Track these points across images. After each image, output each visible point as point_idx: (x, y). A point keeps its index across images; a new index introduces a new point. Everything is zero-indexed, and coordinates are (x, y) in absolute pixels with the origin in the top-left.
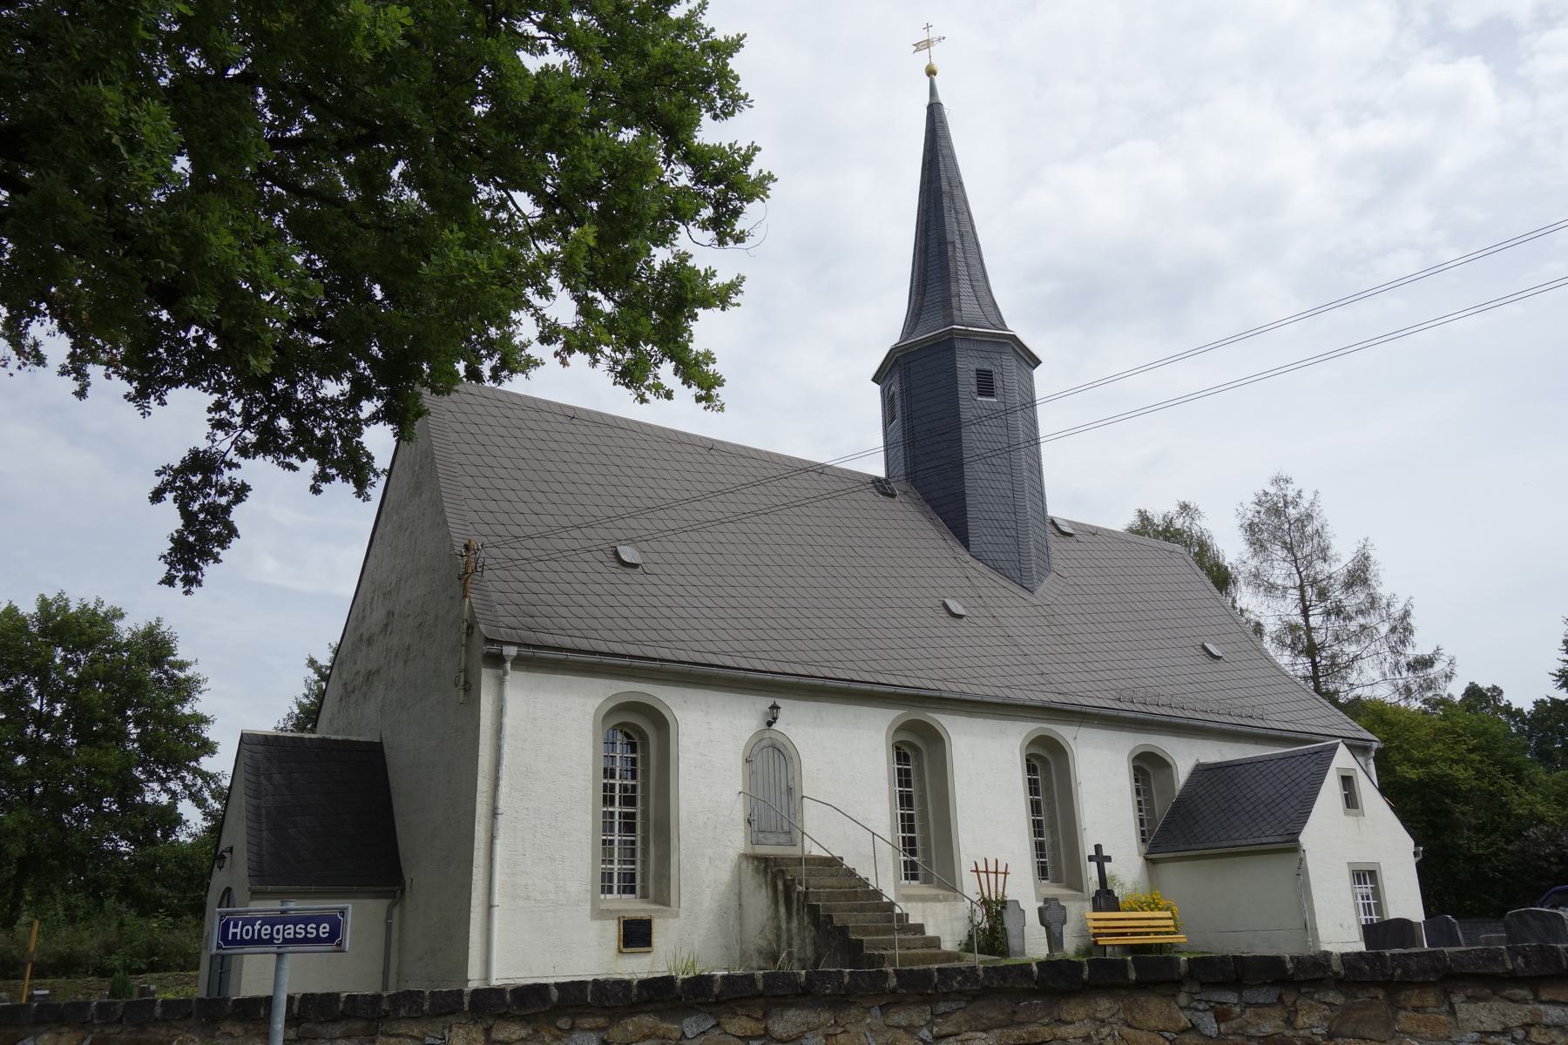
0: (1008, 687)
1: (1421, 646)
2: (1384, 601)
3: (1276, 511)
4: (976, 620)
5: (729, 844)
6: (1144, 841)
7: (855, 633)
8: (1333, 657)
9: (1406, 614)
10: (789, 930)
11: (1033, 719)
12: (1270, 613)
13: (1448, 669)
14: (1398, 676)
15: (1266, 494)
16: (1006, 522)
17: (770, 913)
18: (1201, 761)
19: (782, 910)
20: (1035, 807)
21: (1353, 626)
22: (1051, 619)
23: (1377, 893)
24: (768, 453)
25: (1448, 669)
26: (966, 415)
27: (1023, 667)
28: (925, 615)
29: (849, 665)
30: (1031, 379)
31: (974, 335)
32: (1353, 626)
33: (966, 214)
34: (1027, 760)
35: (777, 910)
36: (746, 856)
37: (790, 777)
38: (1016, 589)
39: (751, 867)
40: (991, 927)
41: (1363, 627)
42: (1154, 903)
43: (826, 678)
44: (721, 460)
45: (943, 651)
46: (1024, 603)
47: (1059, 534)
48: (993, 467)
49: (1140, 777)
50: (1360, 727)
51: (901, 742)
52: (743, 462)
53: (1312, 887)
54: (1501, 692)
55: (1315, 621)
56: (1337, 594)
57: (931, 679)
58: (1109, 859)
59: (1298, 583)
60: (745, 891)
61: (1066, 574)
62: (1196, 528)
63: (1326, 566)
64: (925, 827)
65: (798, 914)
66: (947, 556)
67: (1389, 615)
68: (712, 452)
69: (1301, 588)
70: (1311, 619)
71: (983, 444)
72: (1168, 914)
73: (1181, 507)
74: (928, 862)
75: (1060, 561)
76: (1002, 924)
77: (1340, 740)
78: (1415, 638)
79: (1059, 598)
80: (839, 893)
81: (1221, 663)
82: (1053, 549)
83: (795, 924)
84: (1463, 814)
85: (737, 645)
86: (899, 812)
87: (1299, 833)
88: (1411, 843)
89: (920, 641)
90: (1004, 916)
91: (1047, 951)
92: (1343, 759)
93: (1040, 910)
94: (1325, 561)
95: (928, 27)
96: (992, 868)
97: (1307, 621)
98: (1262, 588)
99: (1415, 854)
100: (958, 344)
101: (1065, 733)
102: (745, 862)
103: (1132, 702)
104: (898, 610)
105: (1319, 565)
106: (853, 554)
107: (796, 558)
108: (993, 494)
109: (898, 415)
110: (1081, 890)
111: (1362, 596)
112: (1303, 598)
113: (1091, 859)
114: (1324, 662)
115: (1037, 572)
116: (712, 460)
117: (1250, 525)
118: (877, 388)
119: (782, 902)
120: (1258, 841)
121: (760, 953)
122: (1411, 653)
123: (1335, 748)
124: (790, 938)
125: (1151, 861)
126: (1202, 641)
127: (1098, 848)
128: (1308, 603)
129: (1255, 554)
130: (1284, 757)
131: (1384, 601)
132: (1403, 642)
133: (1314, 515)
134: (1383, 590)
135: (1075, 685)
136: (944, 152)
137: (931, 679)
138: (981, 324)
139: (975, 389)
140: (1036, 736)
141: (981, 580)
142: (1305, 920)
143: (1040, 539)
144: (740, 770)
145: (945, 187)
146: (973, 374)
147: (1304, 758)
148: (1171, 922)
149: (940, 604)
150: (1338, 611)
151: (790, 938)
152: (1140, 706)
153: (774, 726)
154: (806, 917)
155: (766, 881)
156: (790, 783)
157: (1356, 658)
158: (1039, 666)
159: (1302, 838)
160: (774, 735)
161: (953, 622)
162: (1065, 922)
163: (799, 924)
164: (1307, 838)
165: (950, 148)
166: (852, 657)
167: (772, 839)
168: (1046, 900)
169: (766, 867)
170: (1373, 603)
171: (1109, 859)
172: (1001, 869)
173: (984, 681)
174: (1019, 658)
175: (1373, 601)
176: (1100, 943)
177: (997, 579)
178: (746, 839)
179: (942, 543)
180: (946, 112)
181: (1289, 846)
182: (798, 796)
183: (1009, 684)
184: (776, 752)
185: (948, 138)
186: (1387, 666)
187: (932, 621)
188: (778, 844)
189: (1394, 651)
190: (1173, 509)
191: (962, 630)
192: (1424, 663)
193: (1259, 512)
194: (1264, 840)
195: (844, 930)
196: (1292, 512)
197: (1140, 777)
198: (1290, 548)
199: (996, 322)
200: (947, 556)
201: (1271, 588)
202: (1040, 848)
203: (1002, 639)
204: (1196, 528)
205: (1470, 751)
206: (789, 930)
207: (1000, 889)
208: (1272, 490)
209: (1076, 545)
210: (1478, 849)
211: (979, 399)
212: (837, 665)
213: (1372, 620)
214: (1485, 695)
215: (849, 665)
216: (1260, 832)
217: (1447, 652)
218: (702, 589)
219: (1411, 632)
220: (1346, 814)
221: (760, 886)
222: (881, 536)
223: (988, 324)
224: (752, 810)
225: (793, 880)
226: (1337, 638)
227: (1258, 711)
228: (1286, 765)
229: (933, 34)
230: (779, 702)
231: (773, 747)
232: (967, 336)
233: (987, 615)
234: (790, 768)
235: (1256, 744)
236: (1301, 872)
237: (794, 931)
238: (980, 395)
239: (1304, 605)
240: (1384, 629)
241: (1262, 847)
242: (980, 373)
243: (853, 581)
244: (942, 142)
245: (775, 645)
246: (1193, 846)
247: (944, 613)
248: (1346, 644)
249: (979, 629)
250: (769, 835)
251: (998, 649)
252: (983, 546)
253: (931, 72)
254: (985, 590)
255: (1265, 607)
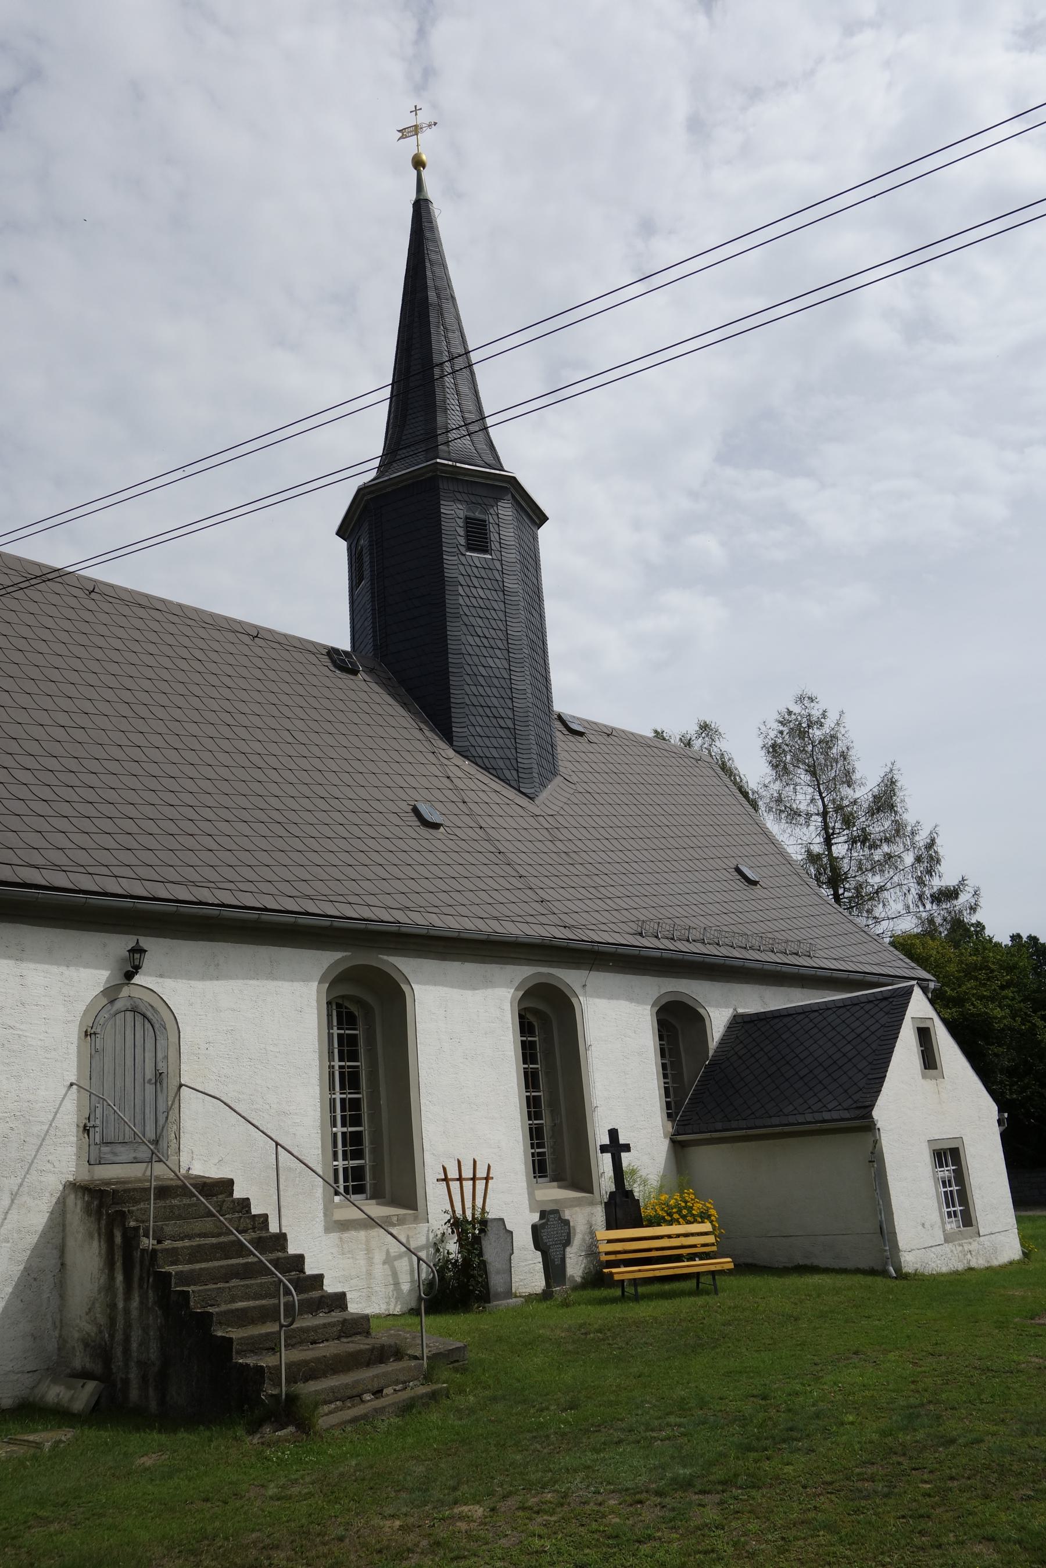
0: (496, 919)
1: (946, 877)
2: (909, 828)
3: (800, 732)
4: (457, 831)
5: (49, 1166)
6: (669, 1116)
7: (279, 843)
8: (859, 888)
9: (931, 845)
10: (127, 1311)
11: (529, 961)
12: (792, 841)
13: (973, 901)
14: (921, 909)
15: (790, 713)
16: (501, 711)
17: (102, 1281)
18: (740, 1011)
19: (119, 1278)
20: (530, 1080)
21: (878, 855)
22: (556, 832)
23: (960, 1177)
24: (180, 605)
25: (973, 901)
26: (450, 572)
27: (517, 892)
28: (387, 823)
29: (265, 887)
30: (535, 538)
31: (465, 475)
32: (878, 855)
33: (458, 333)
34: (521, 1016)
35: (111, 1278)
36: (74, 1187)
37: (160, 1055)
38: (511, 794)
39: (79, 1203)
40: (464, 1259)
41: (889, 857)
42: (686, 1207)
43: (223, 905)
44: (106, 607)
45: (409, 871)
46: (522, 813)
47: (566, 732)
48: (484, 640)
49: (665, 1033)
50: (913, 965)
51: (343, 997)
52: (141, 612)
53: (890, 1178)
54: (984, 928)
55: (840, 849)
56: (862, 821)
57: (387, 908)
58: (627, 1148)
59: (821, 810)
60: (71, 1243)
61: (574, 779)
62: (715, 749)
63: (850, 791)
64: (375, 1116)
65: (141, 1287)
66: (423, 749)
67: (913, 844)
68: (93, 595)
69: (824, 814)
70: (834, 848)
71: (472, 610)
72: (707, 1227)
73: (701, 727)
74: (377, 1169)
75: (568, 764)
76: (481, 1254)
77: (915, 982)
78: (941, 868)
79: (566, 807)
80: (213, 1246)
81: (758, 891)
82: (559, 748)
83: (135, 1303)
84: (996, 1055)
85: (82, 857)
86: (338, 1096)
87: (872, 1106)
88: (994, 1108)
89: (375, 856)
90: (483, 1242)
91: (543, 1283)
92: (919, 1007)
93: (535, 1228)
94: (849, 786)
95: (416, 110)
96: (467, 1173)
97: (830, 850)
98: (783, 816)
99: (1000, 1122)
100: (443, 485)
101: (570, 978)
102: (72, 1196)
103: (657, 937)
104: (348, 815)
105: (845, 791)
106: (290, 739)
107: (203, 740)
108: (484, 674)
109: (367, 573)
110: (590, 1191)
111: (887, 824)
112: (826, 827)
113: (604, 1149)
114: (847, 894)
115: (539, 774)
116: (91, 605)
117: (774, 746)
118: (342, 545)
119: (119, 1265)
120: (818, 1117)
121: (86, 1345)
122: (936, 883)
123: (908, 993)
124: (128, 1326)
125: (678, 1146)
126: (735, 863)
127: (613, 1134)
128: (831, 831)
129: (779, 777)
130: (844, 1005)
131: (909, 828)
132: (929, 872)
133: (840, 736)
134: (909, 818)
135: (584, 915)
136: (433, 256)
137: (387, 908)
138: (471, 461)
139: (462, 541)
140: (531, 985)
141: (467, 781)
142: (881, 1222)
143: (543, 735)
144: (73, 1049)
145: (432, 295)
146: (461, 522)
147: (871, 1005)
148: (711, 1239)
149: (409, 809)
150: (863, 839)
151: (128, 1326)
152: (666, 942)
153: (138, 979)
154: (151, 1293)
155: (99, 1228)
156: (161, 1066)
157: (881, 889)
158: (539, 891)
159: (876, 1113)
160: (136, 993)
161: (425, 832)
162: (568, 1242)
163: (141, 1303)
164: (882, 1112)
165: (440, 253)
166: (270, 876)
167: (125, 1153)
168: (543, 1214)
169: (100, 1206)
170: (898, 831)
171: (627, 1148)
172: (481, 1173)
173: (463, 910)
174: (513, 880)
175: (899, 828)
176: (617, 1277)
177: (487, 780)
178: (79, 1157)
179: (418, 734)
180: (436, 213)
181: (867, 1126)
182: (173, 1084)
183: (497, 914)
184: (139, 1018)
185: (437, 241)
186: (910, 898)
187: (397, 831)
188: (136, 1161)
189: (920, 882)
190: (692, 729)
191: (437, 843)
192: (949, 894)
193: (781, 732)
194: (827, 1116)
195: (205, 1320)
196: (817, 733)
197: (665, 1033)
198: (812, 771)
199: (490, 459)
200: (423, 749)
201: (793, 815)
202: (535, 1135)
203: (491, 856)
204: (715, 749)
205: (1002, 987)
206: (127, 1311)
207: (479, 1202)
208: (796, 709)
209: (587, 745)
210: (1011, 1094)
211: (468, 554)
212: (243, 886)
213: (896, 849)
214: (968, 930)
215: (265, 887)
216: (820, 1105)
217: (972, 883)
218: (274, 854)
219: (938, 861)
220: (924, 1077)
221: (91, 1236)
222: (405, 785)
223: (481, 463)
224: (93, 1110)
225: (137, 1229)
226: (860, 869)
227: (805, 947)
228: (848, 1014)
229: (423, 118)
230: (145, 942)
231: (134, 1010)
232: (455, 475)
233: (473, 824)
234: (161, 1042)
235: (803, 987)
236: (875, 1160)
237: (135, 1313)
238: (469, 549)
239: (827, 832)
240: (909, 859)
241: (825, 1126)
242: (469, 522)
243: (287, 774)
244: (430, 246)
245: (148, 857)
246: (734, 1124)
247: (414, 821)
248: (870, 875)
249: (460, 843)
250: (119, 1149)
251: (484, 868)
252: (471, 739)
253: (418, 163)
254: (471, 794)
255: (786, 835)
